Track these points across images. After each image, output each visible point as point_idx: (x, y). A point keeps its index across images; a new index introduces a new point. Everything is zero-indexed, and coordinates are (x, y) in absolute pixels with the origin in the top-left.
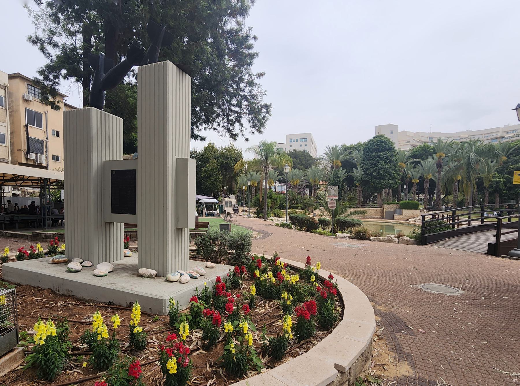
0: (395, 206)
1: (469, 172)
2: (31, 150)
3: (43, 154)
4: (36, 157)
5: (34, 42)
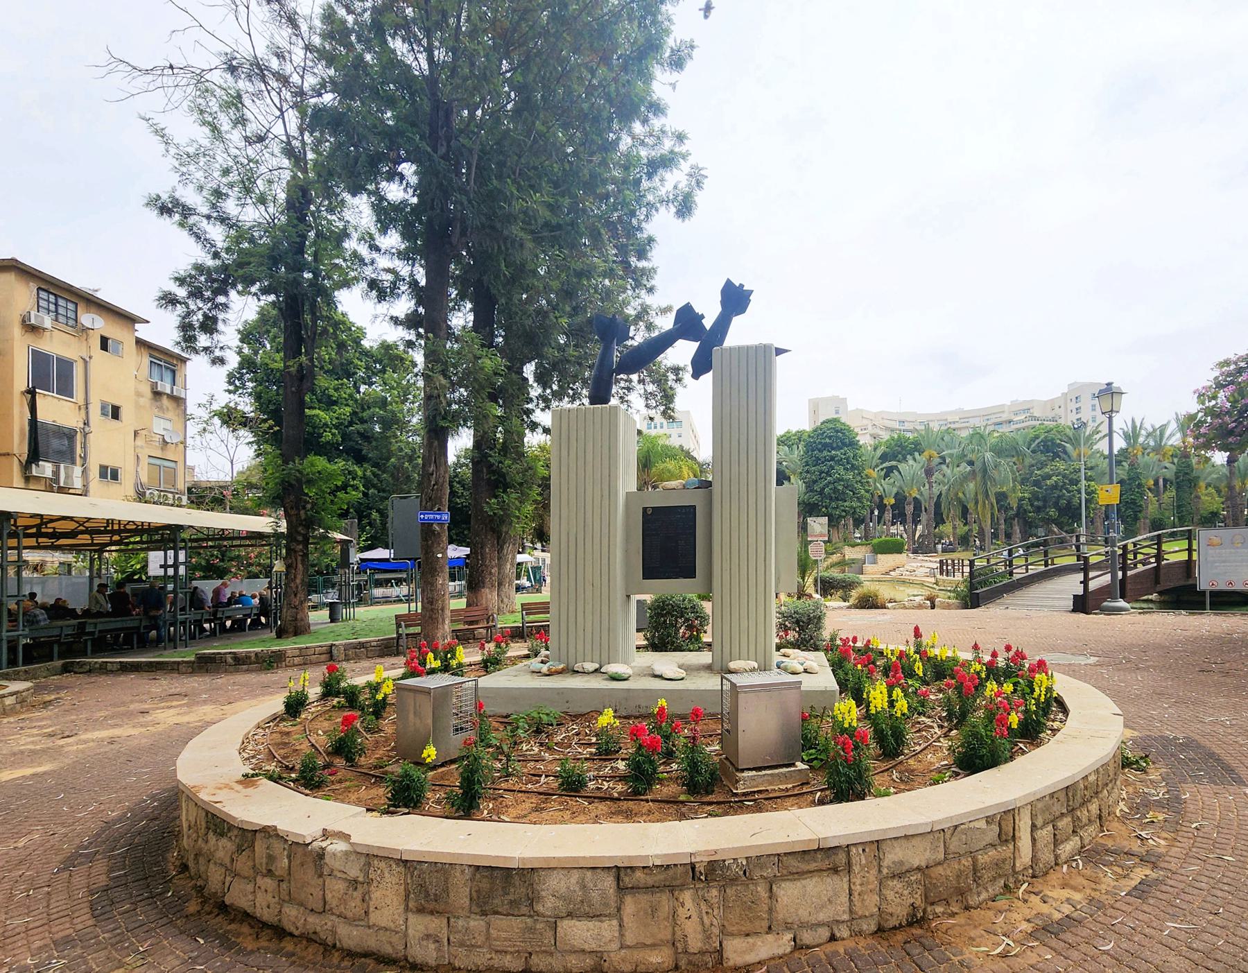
0: (863, 549)
1: (985, 483)
2: (41, 449)
3: (74, 463)
4: (56, 473)
5: (165, 210)
